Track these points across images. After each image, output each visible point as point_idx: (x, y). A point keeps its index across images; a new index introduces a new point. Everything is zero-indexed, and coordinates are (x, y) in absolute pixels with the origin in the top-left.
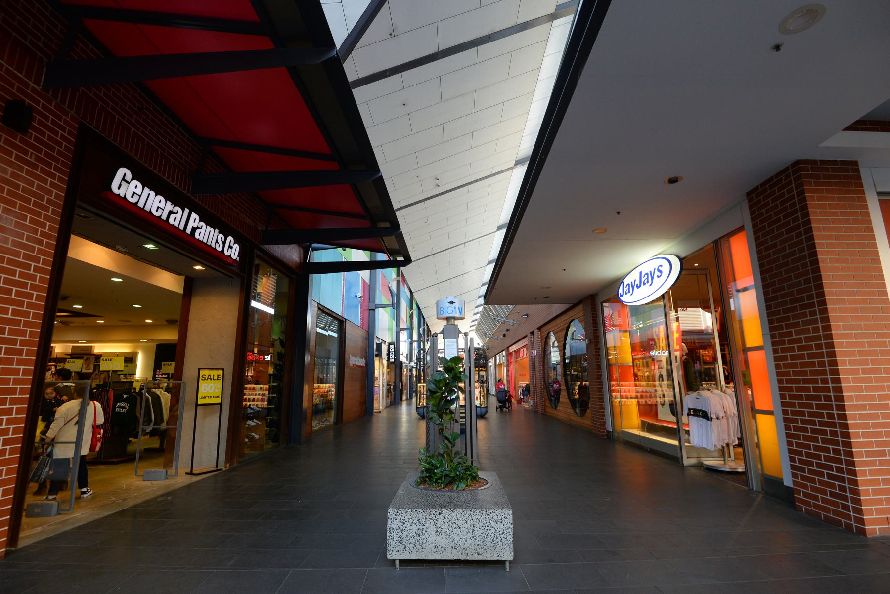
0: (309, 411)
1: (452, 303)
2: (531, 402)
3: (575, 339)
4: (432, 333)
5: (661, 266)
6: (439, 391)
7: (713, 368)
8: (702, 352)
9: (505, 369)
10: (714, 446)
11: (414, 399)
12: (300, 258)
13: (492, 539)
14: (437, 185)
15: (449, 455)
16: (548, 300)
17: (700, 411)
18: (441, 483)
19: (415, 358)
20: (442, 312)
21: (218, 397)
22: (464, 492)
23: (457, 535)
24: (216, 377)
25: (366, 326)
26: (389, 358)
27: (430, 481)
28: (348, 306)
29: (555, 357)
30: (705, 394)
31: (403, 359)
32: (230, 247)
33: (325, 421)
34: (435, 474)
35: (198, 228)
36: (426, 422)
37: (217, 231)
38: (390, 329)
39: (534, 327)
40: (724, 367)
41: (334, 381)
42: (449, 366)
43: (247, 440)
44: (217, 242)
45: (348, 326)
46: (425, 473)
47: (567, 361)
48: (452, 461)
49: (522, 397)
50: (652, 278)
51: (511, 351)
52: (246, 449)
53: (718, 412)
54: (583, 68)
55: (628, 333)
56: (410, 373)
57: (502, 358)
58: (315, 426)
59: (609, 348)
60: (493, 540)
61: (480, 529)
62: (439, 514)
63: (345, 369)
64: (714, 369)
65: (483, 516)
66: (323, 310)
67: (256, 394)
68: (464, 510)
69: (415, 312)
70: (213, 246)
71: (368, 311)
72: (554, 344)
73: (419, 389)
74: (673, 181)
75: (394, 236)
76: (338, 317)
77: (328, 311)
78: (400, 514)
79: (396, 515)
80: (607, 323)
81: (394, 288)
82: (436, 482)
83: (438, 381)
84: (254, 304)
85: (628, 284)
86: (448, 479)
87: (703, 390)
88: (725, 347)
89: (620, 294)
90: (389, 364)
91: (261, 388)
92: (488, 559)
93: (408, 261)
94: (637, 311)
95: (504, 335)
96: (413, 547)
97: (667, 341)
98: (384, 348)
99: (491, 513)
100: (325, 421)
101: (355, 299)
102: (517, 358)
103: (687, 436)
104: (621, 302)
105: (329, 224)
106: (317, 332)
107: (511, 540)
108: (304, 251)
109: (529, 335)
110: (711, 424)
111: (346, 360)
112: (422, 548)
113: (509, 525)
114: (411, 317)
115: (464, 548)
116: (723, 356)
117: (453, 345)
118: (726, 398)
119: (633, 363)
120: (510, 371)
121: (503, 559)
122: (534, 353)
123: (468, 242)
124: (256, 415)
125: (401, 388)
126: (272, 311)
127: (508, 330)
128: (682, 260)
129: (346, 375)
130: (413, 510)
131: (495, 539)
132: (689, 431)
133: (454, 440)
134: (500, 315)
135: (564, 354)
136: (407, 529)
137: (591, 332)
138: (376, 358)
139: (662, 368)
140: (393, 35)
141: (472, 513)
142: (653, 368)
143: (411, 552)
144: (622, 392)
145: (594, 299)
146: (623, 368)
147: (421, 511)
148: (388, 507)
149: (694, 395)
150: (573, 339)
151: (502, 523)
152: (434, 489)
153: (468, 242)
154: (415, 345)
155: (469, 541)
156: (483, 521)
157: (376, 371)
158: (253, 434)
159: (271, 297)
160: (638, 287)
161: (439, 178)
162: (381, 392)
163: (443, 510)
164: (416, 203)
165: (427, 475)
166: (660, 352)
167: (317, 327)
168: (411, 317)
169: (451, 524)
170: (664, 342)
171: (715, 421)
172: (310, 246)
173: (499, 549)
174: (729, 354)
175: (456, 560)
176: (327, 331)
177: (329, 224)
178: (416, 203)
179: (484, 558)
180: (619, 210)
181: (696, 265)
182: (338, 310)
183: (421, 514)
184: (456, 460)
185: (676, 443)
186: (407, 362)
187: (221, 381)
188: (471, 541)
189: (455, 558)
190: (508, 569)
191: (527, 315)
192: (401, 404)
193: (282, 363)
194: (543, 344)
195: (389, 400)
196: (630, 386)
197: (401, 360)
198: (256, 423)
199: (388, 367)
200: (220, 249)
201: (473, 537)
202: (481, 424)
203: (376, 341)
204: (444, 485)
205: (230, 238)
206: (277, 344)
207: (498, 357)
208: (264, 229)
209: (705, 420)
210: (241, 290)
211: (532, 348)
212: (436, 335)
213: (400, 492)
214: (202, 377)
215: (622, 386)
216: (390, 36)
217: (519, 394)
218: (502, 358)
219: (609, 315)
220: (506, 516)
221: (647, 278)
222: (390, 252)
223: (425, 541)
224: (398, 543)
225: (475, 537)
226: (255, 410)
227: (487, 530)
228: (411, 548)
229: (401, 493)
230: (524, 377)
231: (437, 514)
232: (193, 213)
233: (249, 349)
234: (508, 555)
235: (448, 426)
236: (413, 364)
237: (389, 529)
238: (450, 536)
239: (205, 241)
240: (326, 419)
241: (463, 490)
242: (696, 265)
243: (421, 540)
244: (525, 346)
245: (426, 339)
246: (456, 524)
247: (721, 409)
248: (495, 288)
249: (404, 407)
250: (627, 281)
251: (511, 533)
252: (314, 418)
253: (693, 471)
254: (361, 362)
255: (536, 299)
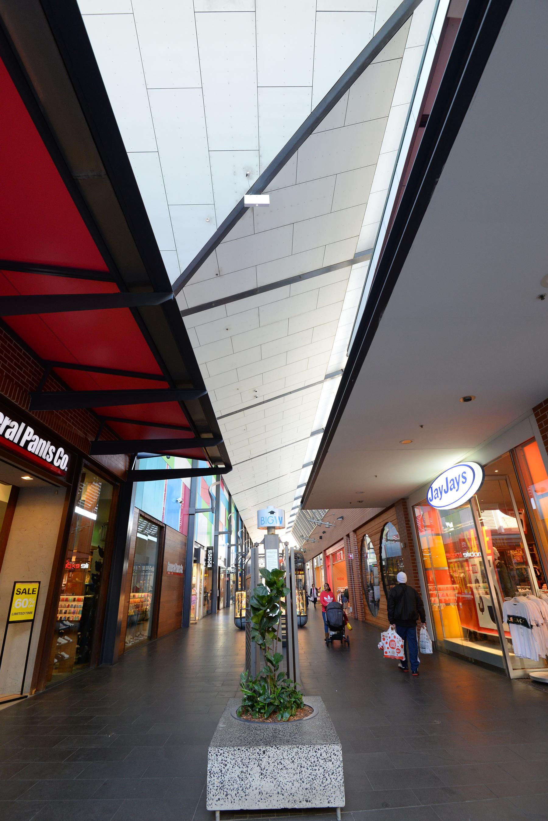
0: (124, 625)
1: (272, 513)
2: (351, 608)
3: (390, 540)
4: (254, 543)
5: (465, 473)
6: (261, 608)
7: (525, 568)
8: (512, 552)
9: (323, 571)
10: (538, 656)
11: (231, 608)
12: (125, 467)
13: (321, 781)
14: (254, 391)
15: (272, 679)
16: (361, 503)
17: (519, 618)
18: (265, 713)
19: (233, 562)
20: (263, 522)
21: (31, 613)
22: (289, 723)
23: (284, 778)
24: (31, 592)
25: (185, 532)
26: (207, 564)
27: (253, 711)
28: (169, 511)
29: (371, 559)
30: (522, 599)
31: (221, 563)
32: (60, 458)
33: (139, 635)
34: (257, 702)
35: (31, 441)
36: (247, 633)
37: (49, 443)
38: (209, 533)
39: (350, 530)
40: (535, 566)
41: (150, 589)
42: (271, 579)
43: (56, 661)
44: (48, 453)
45: (168, 532)
46: (247, 701)
47: (384, 563)
48: (275, 686)
49: (341, 603)
50: (458, 484)
51: (328, 554)
52: (54, 671)
53: (537, 620)
54: (383, 313)
55: (441, 537)
56: (227, 579)
57: (319, 561)
58: (128, 642)
59: (424, 550)
60: (322, 782)
61: (307, 769)
62: (264, 752)
63: (163, 577)
64: (526, 570)
65: (311, 754)
66: (143, 516)
67: (69, 605)
68: (290, 746)
69: (233, 515)
70: (44, 457)
71: (188, 516)
72: (369, 544)
73: (237, 597)
74: (467, 399)
75: (216, 446)
76: (159, 523)
77: (149, 518)
78: (221, 754)
79: (217, 755)
80: (419, 524)
81: (214, 492)
82: (259, 712)
83: (262, 597)
84: (78, 510)
85: (436, 489)
86: (272, 708)
87: (520, 595)
88: (533, 546)
89: (430, 498)
90: (207, 570)
91: (74, 600)
92: (318, 807)
93: (229, 468)
94: (446, 514)
95: (321, 538)
96: (236, 794)
97: (478, 541)
98: (203, 554)
99: (319, 750)
100: (139, 635)
101: (176, 503)
102: (334, 561)
103: (509, 644)
104: (430, 505)
105: (156, 435)
106: (137, 537)
107: (342, 782)
108: (129, 459)
109: (345, 538)
110: (531, 632)
111: (164, 567)
112: (246, 796)
113: (339, 763)
114: (230, 520)
115: (291, 794)
116: (533, 556)
117: (274, 556)
118: (543, 604)
119: (449, 567)
120: (328, 574)
121: (334, 806)
122: (351, 556)
123: (283, 447)
124: (68, 631)
125: (218, 595)
126: (93, 517)
127: (324, 532)
128: (483, 467)
129: (163, 584)
130: (235, 748)
131: (324, 781)
132: (511, 640)
133: (277, 662)
134: (316, 517)
135: (381, 557)
136: (229, 772)
137: (405, 536)
138: (194, 564)
139: (476, 573)
140: (219, 275)
141: (299, 750)
142: (467, 569)
143: (233, 801)
144: (440, 596)
145: (406, 502)
146: (439, 572)
147: (244, 750)
148: (208, 745)
149: (512, 601)
150: (387, 540)
151: (331, 761)
152: (257, 720)
153: (283, 447)
154: (233, 549)
155: (297, 784)
156: (310, 759)
157: (193, 578)
158: (63, 653)
159: (92, 501)
160: (446, 492)
161: (257, 390)
162: (198, 601)
163: (268, 747)
164: (236, 412)
165: (250, 704)
166: (473, 553)
167: (138, 532)
168: (230, 520)
169: (276, 765)
170: (475, 541)
171: (535, 627)
172: (136, 454)
173: (328, 794)
174: (538, 553)
175: (282, 809)
176: (147, 536)
177: (156, 435)
178: (236, 412)
179: (313, 806)
180: (422, 424)
181: (496, 471)
182: (158, 516)
183: (245, 753)
184: (280, 683)
185: (499, 653)
186: (224, 567)
187: (36, 594)
188: (299, 785)
189: (282, 807)
190: (339, 819)
191: (342, 517)
192: (218, 613)
193: (99, 574)
194: (360, 547)
195: (206, 609)
196: (447, 589)
197: (219, 565)
198: (67, 640)
199: (206, 573)
200: (49, 460)
201: (301, 779)
202: (300, 635)
203: (195, 546)
204: (267, 716)
205: (61, 450)
206: (96, 552)
207: (315, 560)
208: (94, 440)
209: (525, 628)
210: (66, 499)
211: (349, 551)
212: (257, 545)
213: (221, 725)
214: (17, 591)
215: (440, 589)
216: (217, 276)
217: (338, 599)
218: (319, 561)
219: (420, 516)
220: (335, 752)
221: (454, 484)
222: (213, 460)
223: (248, 786)
224: (219, 790)
225: (303, 780)
226: (67, 626)
227: (316, 770)
228: (234, 795)
229: (222, 726)
230: (342, 580)
231: (261, 752)
232: (28, 427)
233: (68, 557)
234: (339, 802)
235: (271, 646)
236: (230, 569)
237: (210, 772)
238: (275, 779)
239: (36, 453)
240: (140, 634)
241: (288, 721)
242: (496, 471)
243: (244, 785)
244: (342, 549)
245: (244, 542)
246: (281, 764)
247: (539, 615)
248: (311, 493)
249: (221, 617)
250: (435, 486)
251: (342, 773)
252: (128, 631)
253: (521, 686)
254: (179, 569)
255: (351, 503)
